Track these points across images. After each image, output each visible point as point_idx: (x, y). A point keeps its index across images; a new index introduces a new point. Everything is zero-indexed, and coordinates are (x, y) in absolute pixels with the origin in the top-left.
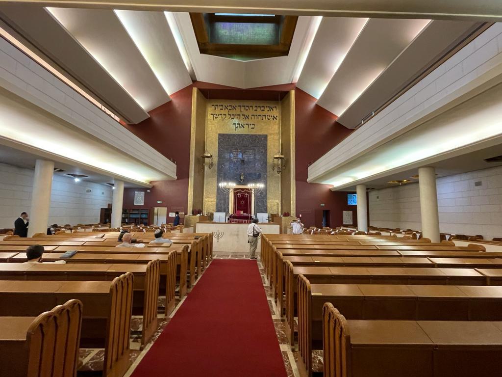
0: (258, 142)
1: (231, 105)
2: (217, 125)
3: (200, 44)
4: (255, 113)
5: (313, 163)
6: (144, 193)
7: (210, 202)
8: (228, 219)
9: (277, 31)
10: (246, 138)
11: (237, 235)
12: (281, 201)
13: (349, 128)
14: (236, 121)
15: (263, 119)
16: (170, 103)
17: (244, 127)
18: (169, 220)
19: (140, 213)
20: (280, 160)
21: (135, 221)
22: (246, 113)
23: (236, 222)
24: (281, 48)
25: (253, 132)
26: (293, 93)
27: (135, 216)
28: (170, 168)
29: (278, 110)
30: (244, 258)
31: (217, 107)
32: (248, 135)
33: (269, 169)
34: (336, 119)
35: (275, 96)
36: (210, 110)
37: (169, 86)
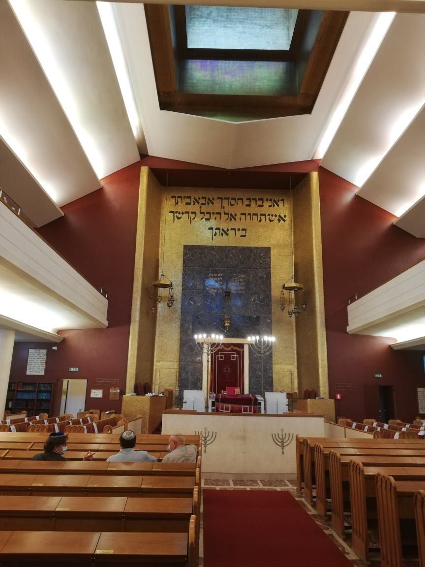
0: (254, 260)
1: (204, 196)
2: (180, 231)
3: (161, 94)
4: (247, 210)
5: (359, 298)
6: (45, 351)
7: (165, 371)
8: (213, 403)
9: (290, 75)
10: (232, 253)
11: (244, 438)
12: (298, 368)
13: (418, 236)
14: (213, 223)
15: (260, 221)
16: (101, 191)
17: (227, 235)
18: (91, 404)
19: (36, 390)
20: (293, 292)
21: (27, 406)
22: (231, 210)
23: (227, 409)
24: (299, 101)
25: (243, 243)
26: (315, 175)
27: (26, 396)
28: (95, 303)
29: (286, 205)
30: (260, 486)
31: (180, 200)
32: (236, 247)
33: (275, 308)
34: (393, 221)
35: (284, 182)
36: (168, 204)
37: (102, 163)
